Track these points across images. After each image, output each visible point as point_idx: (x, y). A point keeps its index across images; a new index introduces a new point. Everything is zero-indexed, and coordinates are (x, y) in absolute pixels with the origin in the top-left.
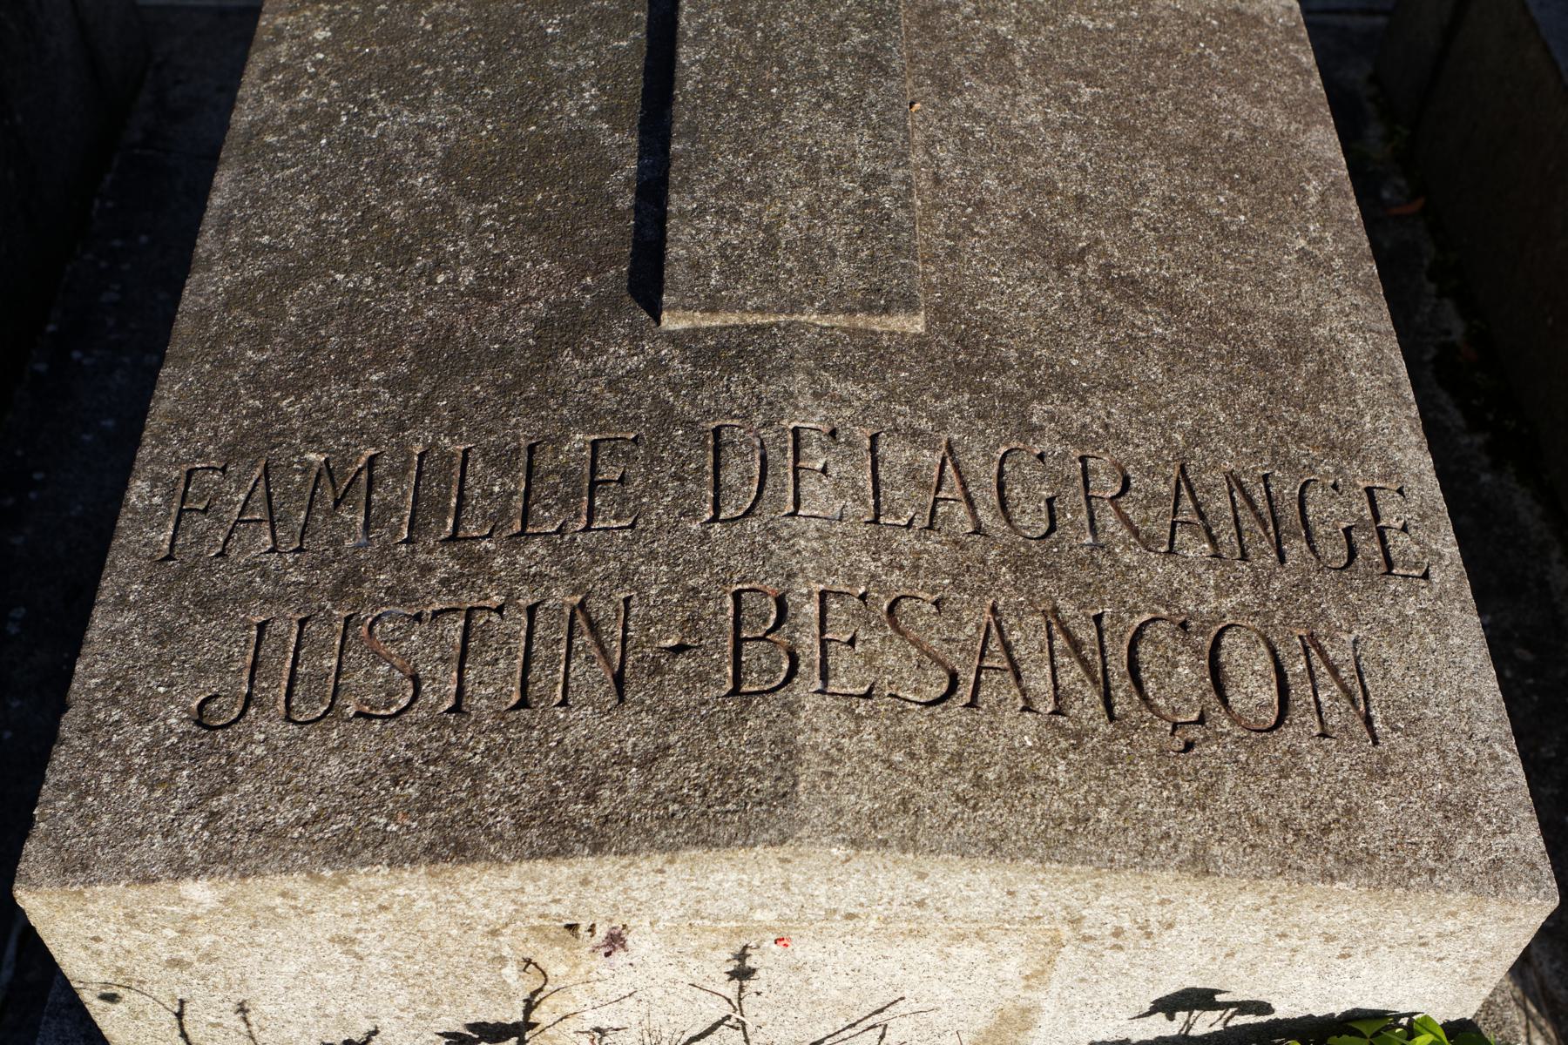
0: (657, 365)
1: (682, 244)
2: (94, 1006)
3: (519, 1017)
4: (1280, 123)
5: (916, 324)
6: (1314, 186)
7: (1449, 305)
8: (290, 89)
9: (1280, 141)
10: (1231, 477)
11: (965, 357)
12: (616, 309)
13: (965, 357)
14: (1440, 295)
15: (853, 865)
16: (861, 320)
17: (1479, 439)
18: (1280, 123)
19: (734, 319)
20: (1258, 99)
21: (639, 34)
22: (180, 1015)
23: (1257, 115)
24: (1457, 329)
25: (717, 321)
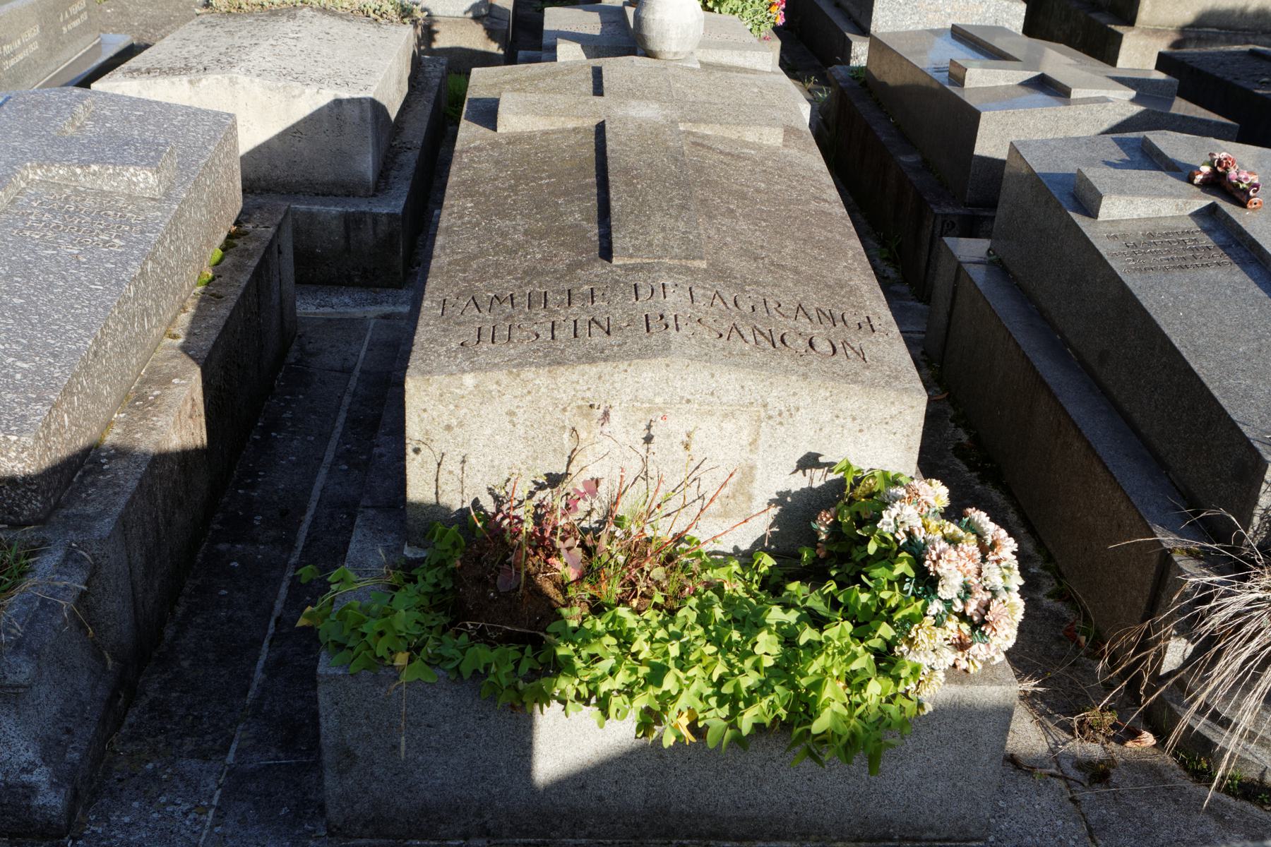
0: (612, 271)
1: (616, 245)
2: (409, 450)
3: (564, 470)
4: (838, 237)
5: (703, 265)
6: (850, 254)
7: (960, 430)
8: (461, 217)
9: (838, 242)
10: (817, 309)
11: (719, 273)
12: (595, 260)
13: (719, 273)
14: (956, 427)
15: (691, 369)
16: (683, 262)
17: (974, 474)
18: (838, 237)
19: (639, 260)
20: (830, 231)
21: (595, 202)
22: (439, 464)
23: (830, 235)
24: (965, 438)
25: (633, 261)
